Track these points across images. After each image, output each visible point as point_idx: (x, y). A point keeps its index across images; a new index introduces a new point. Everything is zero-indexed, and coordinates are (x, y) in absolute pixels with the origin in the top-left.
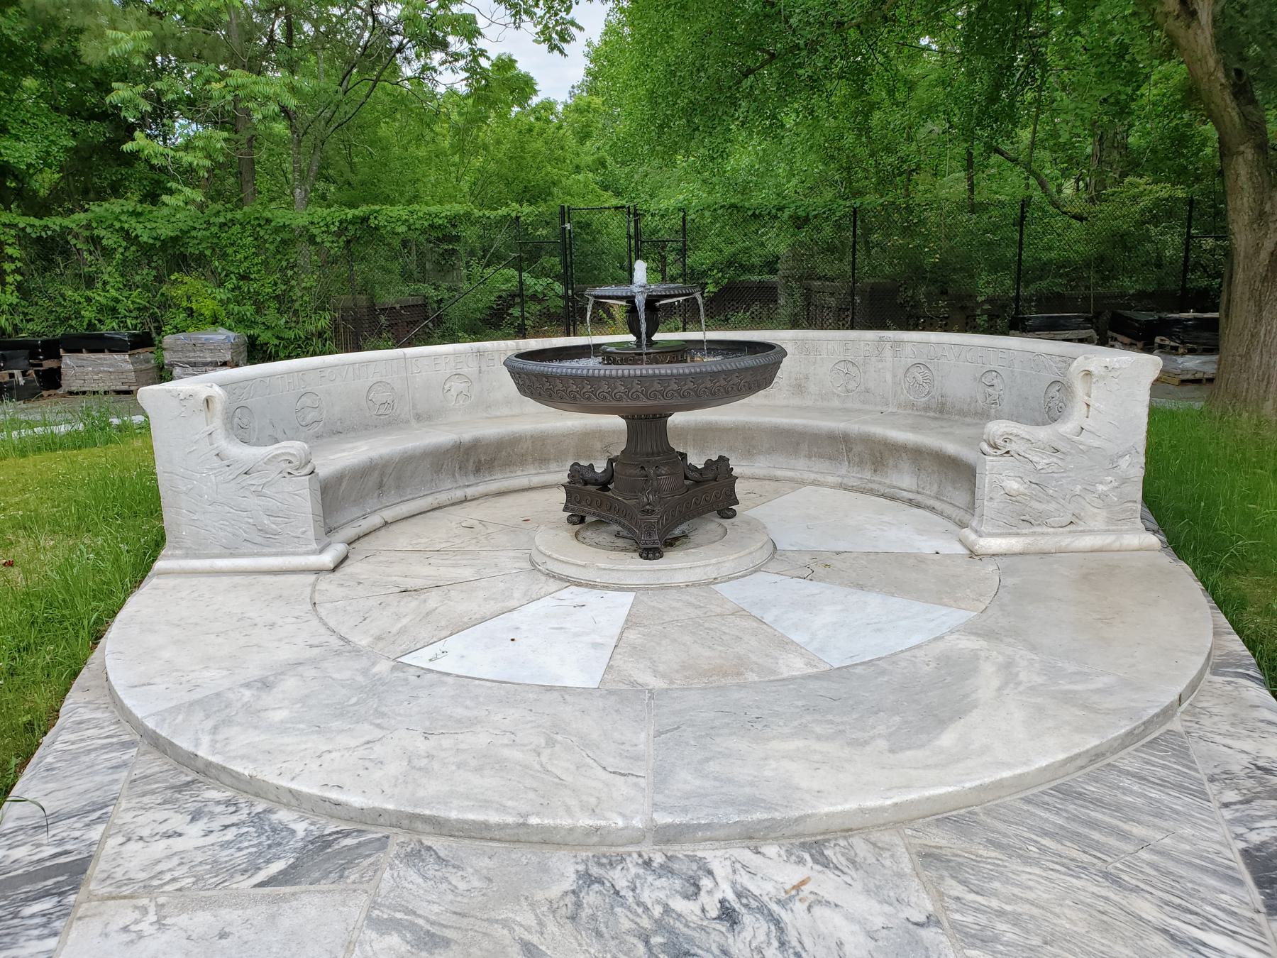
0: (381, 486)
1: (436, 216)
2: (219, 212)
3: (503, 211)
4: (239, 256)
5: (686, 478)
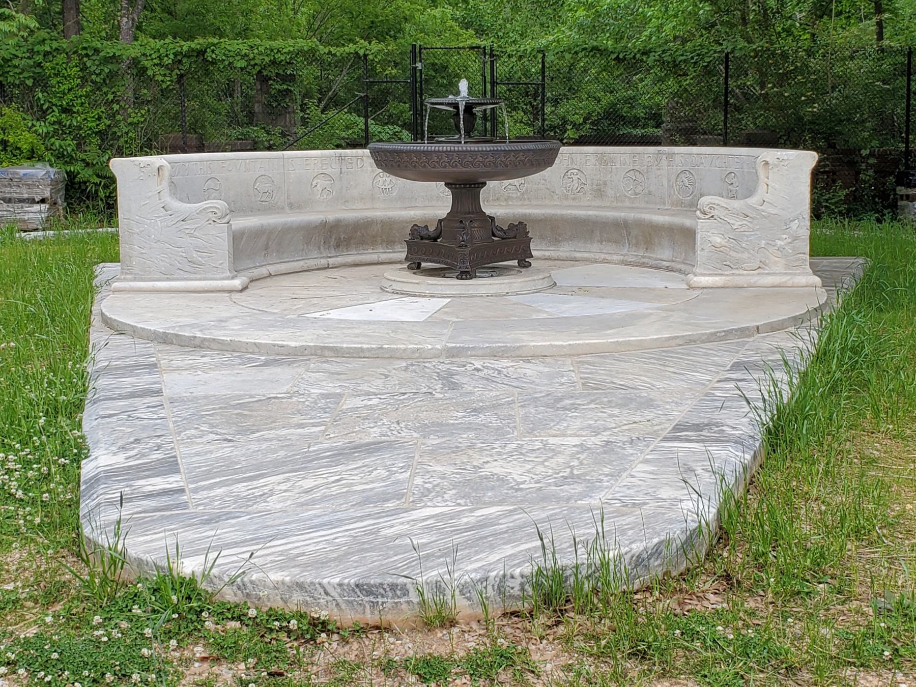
0: (267, 248)
1: (279, 51)
2: (44, 40)
3: (350, 48)
4: (62, 88)
5: (494, 236)
